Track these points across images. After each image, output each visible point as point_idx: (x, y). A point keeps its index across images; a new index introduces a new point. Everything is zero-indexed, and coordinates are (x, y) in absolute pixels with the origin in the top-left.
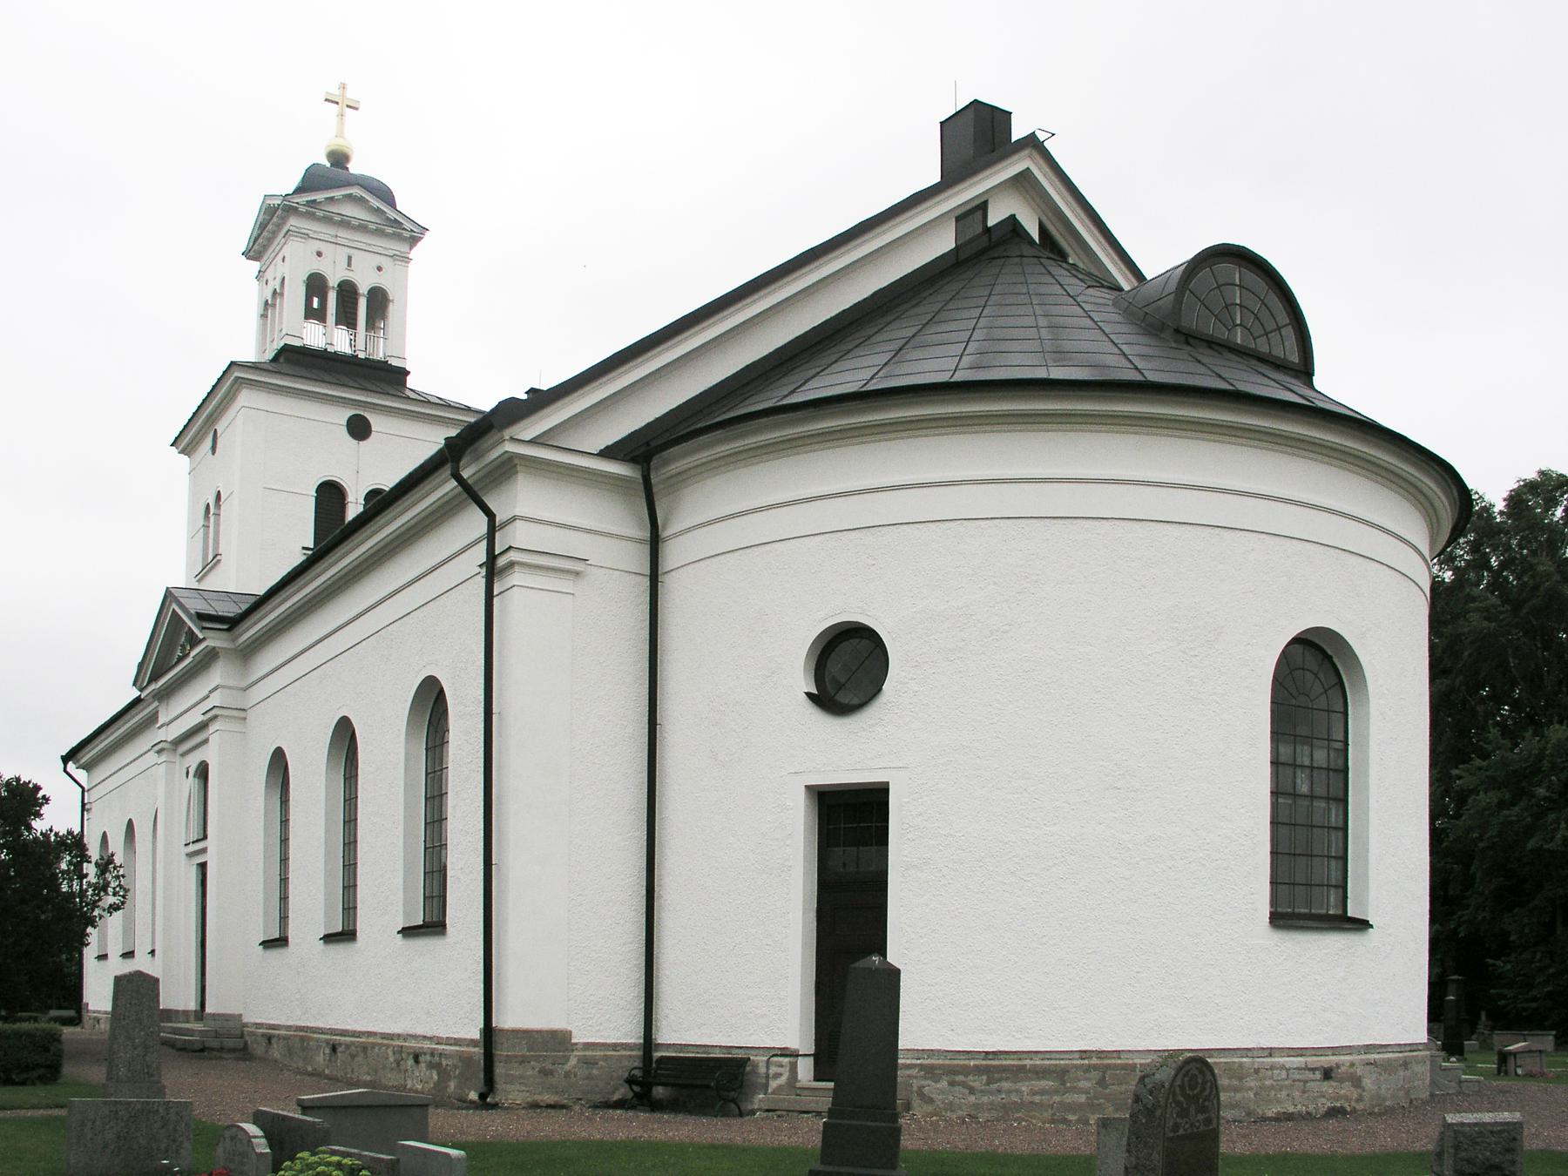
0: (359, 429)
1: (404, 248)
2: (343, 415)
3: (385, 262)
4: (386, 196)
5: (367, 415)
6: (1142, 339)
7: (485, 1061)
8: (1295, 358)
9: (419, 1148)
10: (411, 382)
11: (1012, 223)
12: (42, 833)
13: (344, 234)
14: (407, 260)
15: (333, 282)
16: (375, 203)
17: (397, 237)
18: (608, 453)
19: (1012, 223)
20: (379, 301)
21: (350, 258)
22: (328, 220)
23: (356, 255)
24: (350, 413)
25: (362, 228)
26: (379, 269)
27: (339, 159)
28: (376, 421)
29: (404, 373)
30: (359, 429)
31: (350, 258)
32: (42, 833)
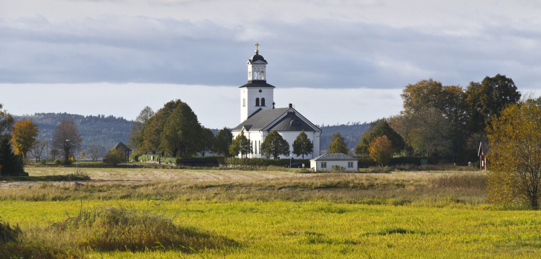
0: (260, 91)
3: (263, 68)
8: (299, 124)
11: (291, 112)
13: (258, 65)
18: (267, 131)
19: (291, 112)
23: (260, 68)
24: (259, 90)
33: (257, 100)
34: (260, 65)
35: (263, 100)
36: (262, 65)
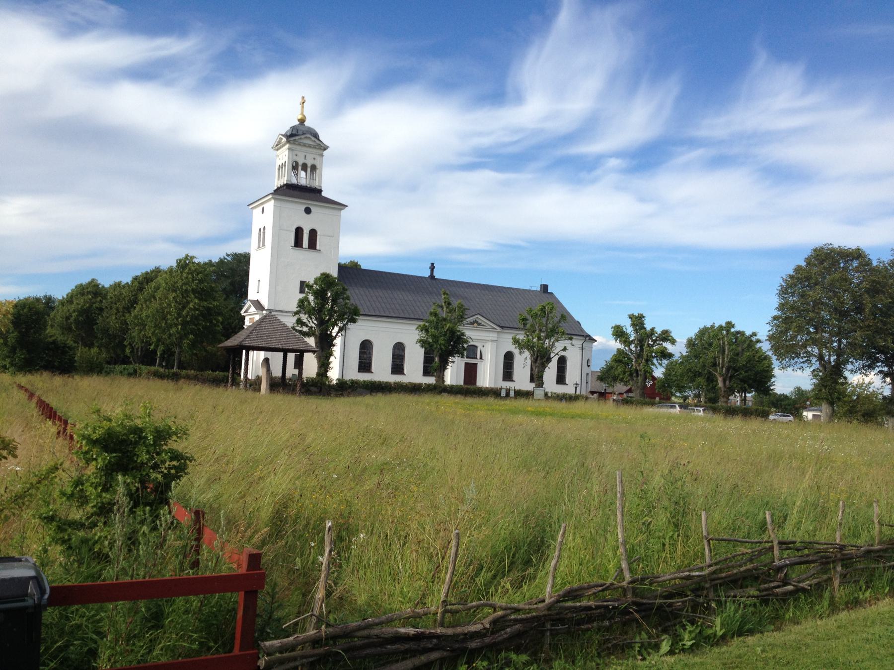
0: (308, 211)
1: (320, 152)
2: (303, 207)
4: (316, 136)
5: (310, 207)
6: (810, 100)
7: (157, 580)
9: (256, 570)
10: (323, 194)
12: (182, 476)
13: (305, 149)
14: (322, 155)
15: (300, 163)
16: (313, 139)
17: (320, 149)
20: (314, 168)
21: (305, 156)
22: (299, 145)
23: (308, 155)
25: (310, 146)
26: (314, 159)
27: (302, 121)
28: (313, 209)
29: (320, 191)
30: (308, 211)
31: (305, 156)
32: (182, 476)
33: (299, 232)
34: (310, 150)
35: (313, 233)
36: (315, 151)
